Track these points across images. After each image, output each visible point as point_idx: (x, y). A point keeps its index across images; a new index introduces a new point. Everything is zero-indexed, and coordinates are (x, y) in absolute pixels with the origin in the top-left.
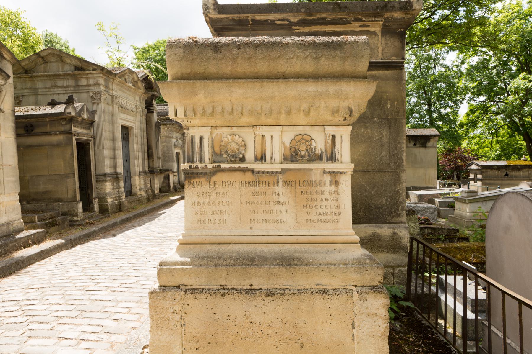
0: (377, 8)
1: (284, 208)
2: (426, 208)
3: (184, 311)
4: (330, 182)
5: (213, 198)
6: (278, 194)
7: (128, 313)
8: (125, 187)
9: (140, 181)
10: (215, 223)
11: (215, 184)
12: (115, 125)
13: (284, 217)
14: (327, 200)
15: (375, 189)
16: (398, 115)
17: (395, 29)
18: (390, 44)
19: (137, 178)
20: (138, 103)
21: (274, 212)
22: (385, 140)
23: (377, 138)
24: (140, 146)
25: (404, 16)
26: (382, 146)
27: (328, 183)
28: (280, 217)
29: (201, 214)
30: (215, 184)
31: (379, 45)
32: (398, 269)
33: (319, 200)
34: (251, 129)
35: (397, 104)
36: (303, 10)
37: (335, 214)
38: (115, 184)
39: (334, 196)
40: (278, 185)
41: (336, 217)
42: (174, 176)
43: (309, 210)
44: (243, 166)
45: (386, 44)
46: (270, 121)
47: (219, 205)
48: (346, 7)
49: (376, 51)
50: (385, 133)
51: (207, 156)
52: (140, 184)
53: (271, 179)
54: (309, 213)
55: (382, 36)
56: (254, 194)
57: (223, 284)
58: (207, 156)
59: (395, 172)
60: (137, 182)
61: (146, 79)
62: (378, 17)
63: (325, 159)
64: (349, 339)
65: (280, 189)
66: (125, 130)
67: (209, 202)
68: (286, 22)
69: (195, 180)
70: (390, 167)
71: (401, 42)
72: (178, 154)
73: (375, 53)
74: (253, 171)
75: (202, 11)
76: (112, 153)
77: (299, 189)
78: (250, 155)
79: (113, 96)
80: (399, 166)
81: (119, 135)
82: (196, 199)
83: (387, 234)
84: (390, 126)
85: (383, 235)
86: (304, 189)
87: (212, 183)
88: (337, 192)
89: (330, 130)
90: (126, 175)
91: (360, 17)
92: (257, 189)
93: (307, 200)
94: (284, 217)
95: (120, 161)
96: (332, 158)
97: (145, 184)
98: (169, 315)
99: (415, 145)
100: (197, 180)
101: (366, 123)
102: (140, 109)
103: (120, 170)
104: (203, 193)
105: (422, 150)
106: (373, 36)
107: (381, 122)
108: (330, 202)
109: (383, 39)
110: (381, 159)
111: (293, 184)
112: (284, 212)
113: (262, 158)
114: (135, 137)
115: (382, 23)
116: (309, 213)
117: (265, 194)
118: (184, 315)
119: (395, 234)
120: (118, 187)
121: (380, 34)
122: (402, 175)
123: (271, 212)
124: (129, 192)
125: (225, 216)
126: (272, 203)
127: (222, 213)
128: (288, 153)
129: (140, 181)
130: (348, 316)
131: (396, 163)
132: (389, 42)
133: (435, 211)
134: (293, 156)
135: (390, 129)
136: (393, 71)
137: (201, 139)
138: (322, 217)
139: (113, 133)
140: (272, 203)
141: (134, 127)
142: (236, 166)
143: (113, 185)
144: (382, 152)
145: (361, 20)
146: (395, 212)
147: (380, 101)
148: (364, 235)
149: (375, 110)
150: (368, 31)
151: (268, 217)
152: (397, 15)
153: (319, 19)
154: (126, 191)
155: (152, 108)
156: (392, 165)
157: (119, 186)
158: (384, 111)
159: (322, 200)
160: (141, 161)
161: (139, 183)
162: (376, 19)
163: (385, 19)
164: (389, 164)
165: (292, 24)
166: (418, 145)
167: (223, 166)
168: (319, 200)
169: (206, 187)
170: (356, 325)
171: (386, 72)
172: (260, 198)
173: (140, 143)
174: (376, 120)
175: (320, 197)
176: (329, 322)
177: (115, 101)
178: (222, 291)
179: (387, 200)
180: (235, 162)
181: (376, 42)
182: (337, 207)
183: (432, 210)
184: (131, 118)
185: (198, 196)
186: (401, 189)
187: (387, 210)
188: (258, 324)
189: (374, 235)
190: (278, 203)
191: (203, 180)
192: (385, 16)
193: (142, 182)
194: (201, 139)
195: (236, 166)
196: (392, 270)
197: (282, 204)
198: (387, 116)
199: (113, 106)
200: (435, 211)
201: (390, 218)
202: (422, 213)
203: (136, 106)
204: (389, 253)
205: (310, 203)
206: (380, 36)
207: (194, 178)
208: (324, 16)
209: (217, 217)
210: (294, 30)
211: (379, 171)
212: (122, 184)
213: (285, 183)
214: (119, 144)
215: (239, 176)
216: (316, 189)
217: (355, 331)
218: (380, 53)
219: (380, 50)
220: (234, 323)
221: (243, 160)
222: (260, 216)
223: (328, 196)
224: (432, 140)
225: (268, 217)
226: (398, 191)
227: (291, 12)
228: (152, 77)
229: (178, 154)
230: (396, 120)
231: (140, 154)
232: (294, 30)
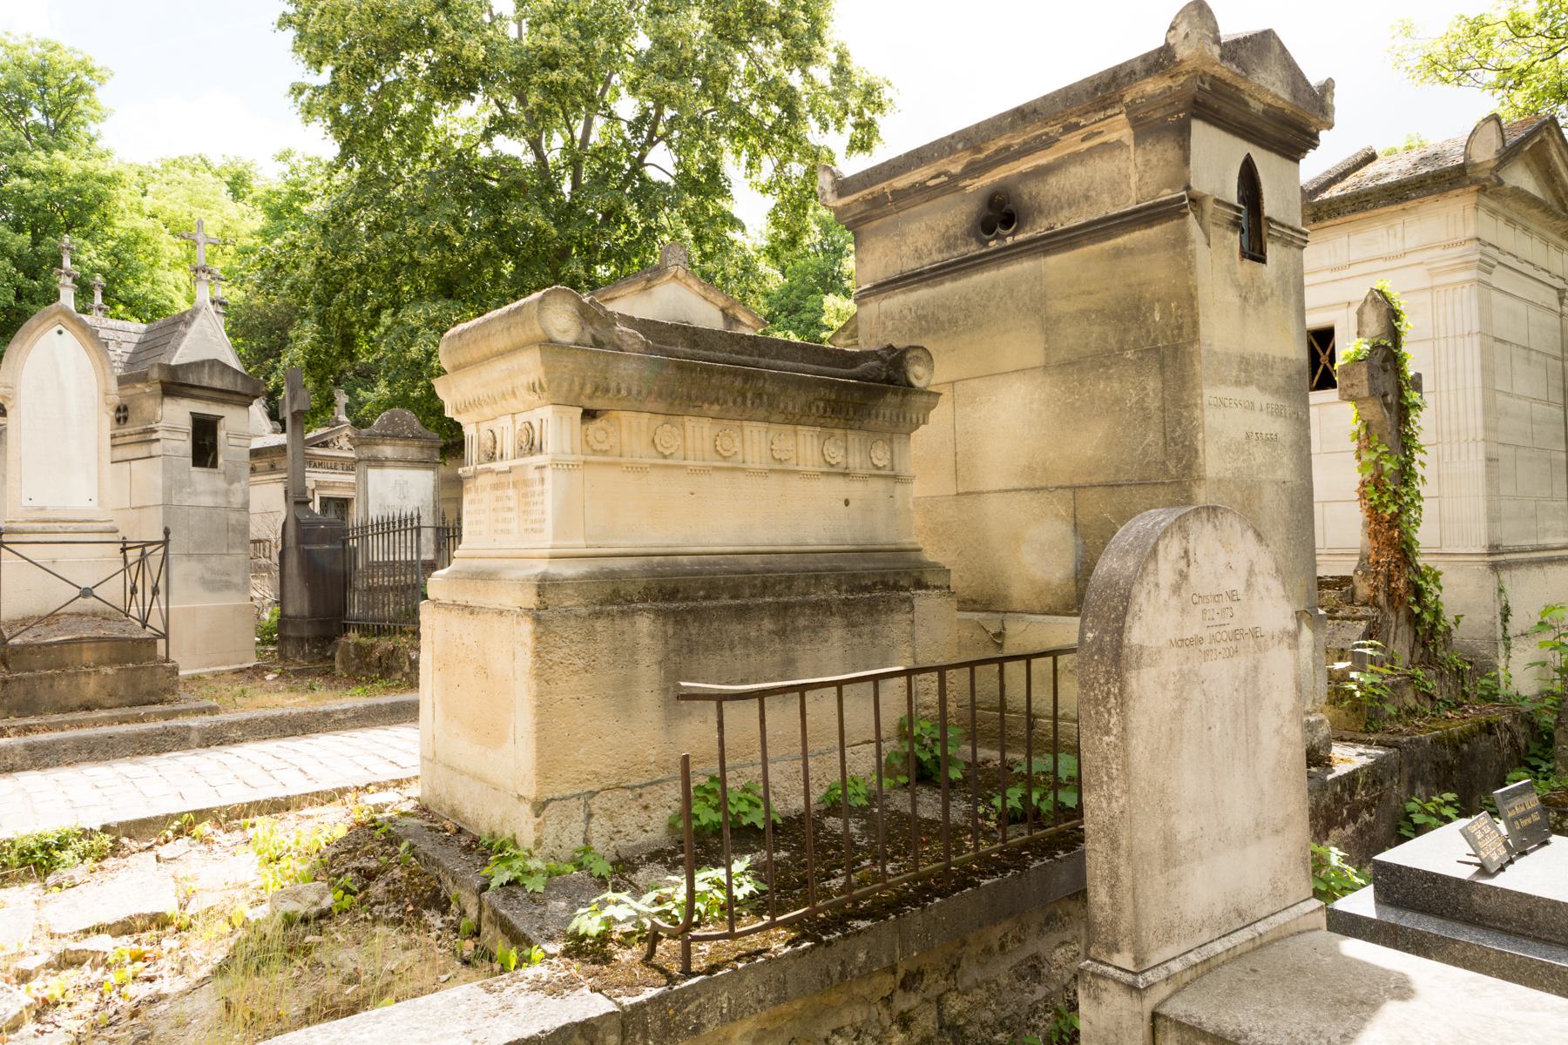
0: (1096, 89)
16: (1180, 335)
17: (1163, 119)
18: (1154, 161)
22: (1153, 404)
25: (1169, 82)
31: (1132, 169)
35: (1178, 308)
36: (960, 146)
48: (1035, 111)
49: (1124, 187)
50: (1153, 384)
55: (1137, 145)
59: (1180, 483)
62: (1111, 105)
68: (943, 179)
70: (1166, 472)
71: (1181, 147)
80: (1189, 467)
84: (1162, 367)
91: (1074, 120)
101: (1109, 368)
107: (1142, 359)
110: (1145, 453)
115: (1123, 116)
122: (1196, 490)
123: (504, 520)
131: (1179, 460)
135: (1162, 374)
136: (1164, 226)
145: (1077, 126)
147: (1138, 308)
149: (1127, 331)
150: (1105, 143)
152: (1152, 86)
153: (997, 152)
156: (1171, 465)
158: (1148, 332)
162: (1109, 112)
163: (1127, 106)
165: (954, 179)
174: (1129, 355)
181: (1123, 165)
192: (1127, 99)
198: (1155, 341)
208: (1002, 143)
211: (1142, 483)
218: (1133, 185)
219: (1134, 179)
227: (941, 157)
230: (1176, 348)
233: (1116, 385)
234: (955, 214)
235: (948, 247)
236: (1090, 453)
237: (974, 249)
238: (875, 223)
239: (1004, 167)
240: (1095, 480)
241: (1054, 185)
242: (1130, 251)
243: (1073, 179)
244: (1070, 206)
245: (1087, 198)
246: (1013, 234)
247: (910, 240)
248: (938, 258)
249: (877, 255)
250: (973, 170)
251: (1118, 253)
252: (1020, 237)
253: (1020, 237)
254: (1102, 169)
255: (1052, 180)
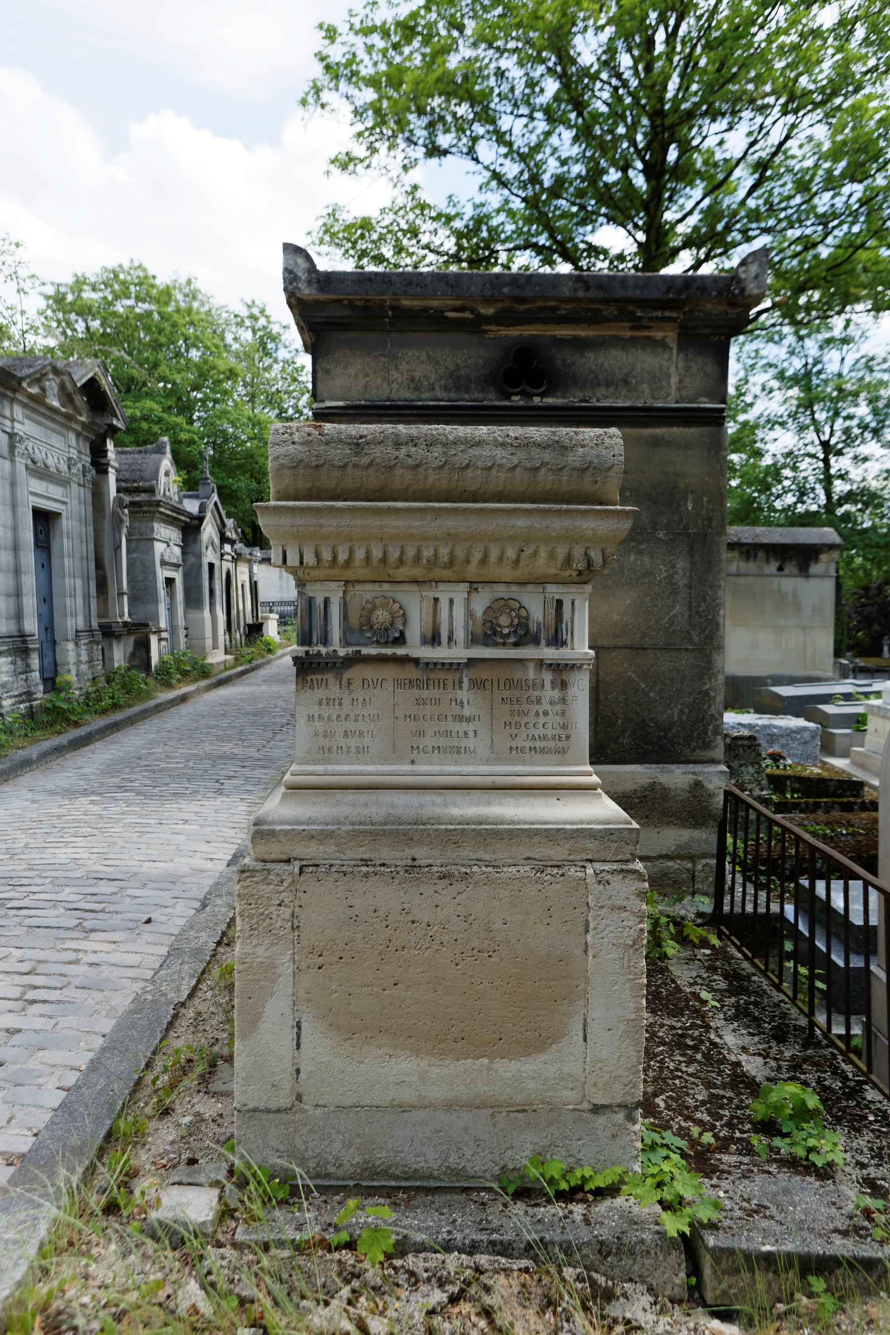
1: (471, 727)
2: (792, 731)
3: (297, 902)
4: (553, 683)
5: (347, 708)
6: (462, 703)
7: (115, 951)
8: (42, 671)
9: (79, 655)
10: (348, 752)
11: (349, 684)
12: (20, 509)
13: (471, 743)
14: (546, 713)
15: (657, 689)
16: (709, 526)
18: (695, 369)
19: (71, 646)
20: (74, 454)
21: (454, 734)
22: (681, 580)
23: (664, 575)
24: (77, 563)
26: (674, 593)
27: (547, 685)
28: (464, 743)
29: (325, 736)
30: (349, 684)
31: (672, 370)
32: (704, 861)
33: (532, 713)
34: (414, 588)
35: (709, 502)
37: (560, 739)
38: (19, 662)
39: (559, 708)
40: (461, 688)
41: (560, 744)
42: (160, 640)
43: (514, 731)
44: (400, 651)
45: (688, 369)
46: (447, 574)
47: (356, 720)
49: (664, 383)
50: (682, 564)
51: (336, 633)
52: (78, 662)
53: (450, 677)
54: (513, 737)
55: (680, 349)
56: (419, 701)
57: (366, 856)
58: (336, 633)
59: (701, 650)
60: (71, 657)
61: (92, 388)
63: (543, 642)
64: (578, 952)
65: (463, 694)
66: (44, 519)
67: (339, 716)
68: (467, 315)
69: (314, 677)
70: (690, 640)
72: (170, 582)
73: (662, 388)
74: (416, 661)
75: (282, 286)
76: (11, 580)
77: (499, 694)
78: (414, 633)
79: (12, 436)
81: (28, 535)
82: (315, 711)
83: (680, 785)
84: (691, 551)
85: (673, 786)
86: (507, 694)
87: (345, 682)
88: (564, 701)
89: (554, 591)
90: (43, 638)
92: (425, 694)
93: (512, 713)
94: (471, 743)
95: (30, 603)
96: (557, 641)
97: (91, 661)
98: (273, 909)
99: (780, 569)
100: (319, 677)
101: (640, 543)
102: (80, 465)
103: (31, 625)
104: (328, 699)
105: (801, 582)
106: (659, 350)
107: (673, 541)
108: (551, 718)
109: (681, 356)
110: (671, 623)
111: (488, 684)
112: (471, 735)
113: (433, 639)
114: (65, 540)
116: (513, 737)
117: (438, 702)
118: (297, 909)
119: (698, 784)
120: (28, 670)
121: (675, 347)
123: (448, 734)
124: (51, 682)
125: (367, 741)
126: (450, 718)
127: (361, 735)
128: (479, 629)
129: (79, 655)
130: (579, 910)
131: (703, 631)
132: (693, 365)
133: (813, 737)
134: (487, 633)
137: (327, 602)
138: (538, 744)
139: (15, 529)
140: (450, 718)
141: (64, 514)
142: (389, 651)
143: (14, 663)
144: (672, 608)
146: (699, 737)
148: (633, 787)
150: (649, 338)
151: (442, 742)
153: (541, 309)
154: (45, 680)
155: (104, 461)
156: (694, 635)
157: (28, 665)
158: (681, 518)
159: (537, 714)
160: (80, 601)
161: (76, 662)
162: (667, 314)
164: (688, 632)
165: (482, 320)
166: (787, 571)
167: (365, 651)
168: (532, 713)
169: (334, 691)
170: (592, 926)
171: (686, 430)
172: (428, 710)
173: (77, 555)
174: (661, 535)
175: (534, 708)
176: (545, 922)
177: (20, 449)
178: (364, 869)
179: (681, 712)
180: (386, 644)
181: (665, 364)
182: (564, 727)
183: (806, 735)
184: (55, 491)
185: (320, 704)
186: (714, 689)
187: (682, 734)
188: (424, 925)
189: (653, 786)
190: (460, 718)
191: (330, 677)
193: (84, 657)
194: (327, 602)
195: (389, 651)
196: (689, 865)
197: (468, 720)
198: (687, 527)
199: (13, 461)
200: (813, 737)
201: (687, 751)
202: (783, 741)
203: (70, 459)
204: (684, 826)
205: (516, 719)
206: (675, 351)
207: (313, 673)
209: (353, 742)
210: (486, 332)
211: (667, 648)
212: (35, 661)
213: (474, 683)
214: (29, 558)
215: (390, 672)
216: (528, 694)
217: (589, 937)
219: (674, 380)
220: (384, 923)
221: (401, 640)
222: (429, 741)
223: (548, 707)
224: (824, 557)
225: (442, 742)
226: (706, 693)
228: (106, 383)
229: (170, 582)
231: (79, 582)
232: (486, 332)
233: (647, 560)
234: (470, 356)
235: (458, 388)
236: (616, 617)
237: (492, 400)
238: (351, 335)
239: (544, 327)
240: (620, 642)
241: (591, 360)
242: (668, 444)
243: (614, 360)
244: (608, 385)
245: (626, 383)
246: (542, 395)
247: (403, 366)
248: (442, 397)
249: (352, 370)
250: (505, 318)
251: (656, 442)
252: (550, 401)
253: (550, 401)
254: (646, 361)
255: (591, 356)
